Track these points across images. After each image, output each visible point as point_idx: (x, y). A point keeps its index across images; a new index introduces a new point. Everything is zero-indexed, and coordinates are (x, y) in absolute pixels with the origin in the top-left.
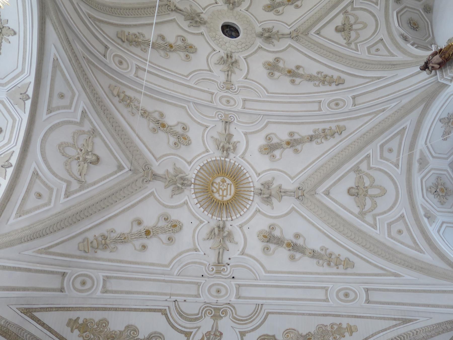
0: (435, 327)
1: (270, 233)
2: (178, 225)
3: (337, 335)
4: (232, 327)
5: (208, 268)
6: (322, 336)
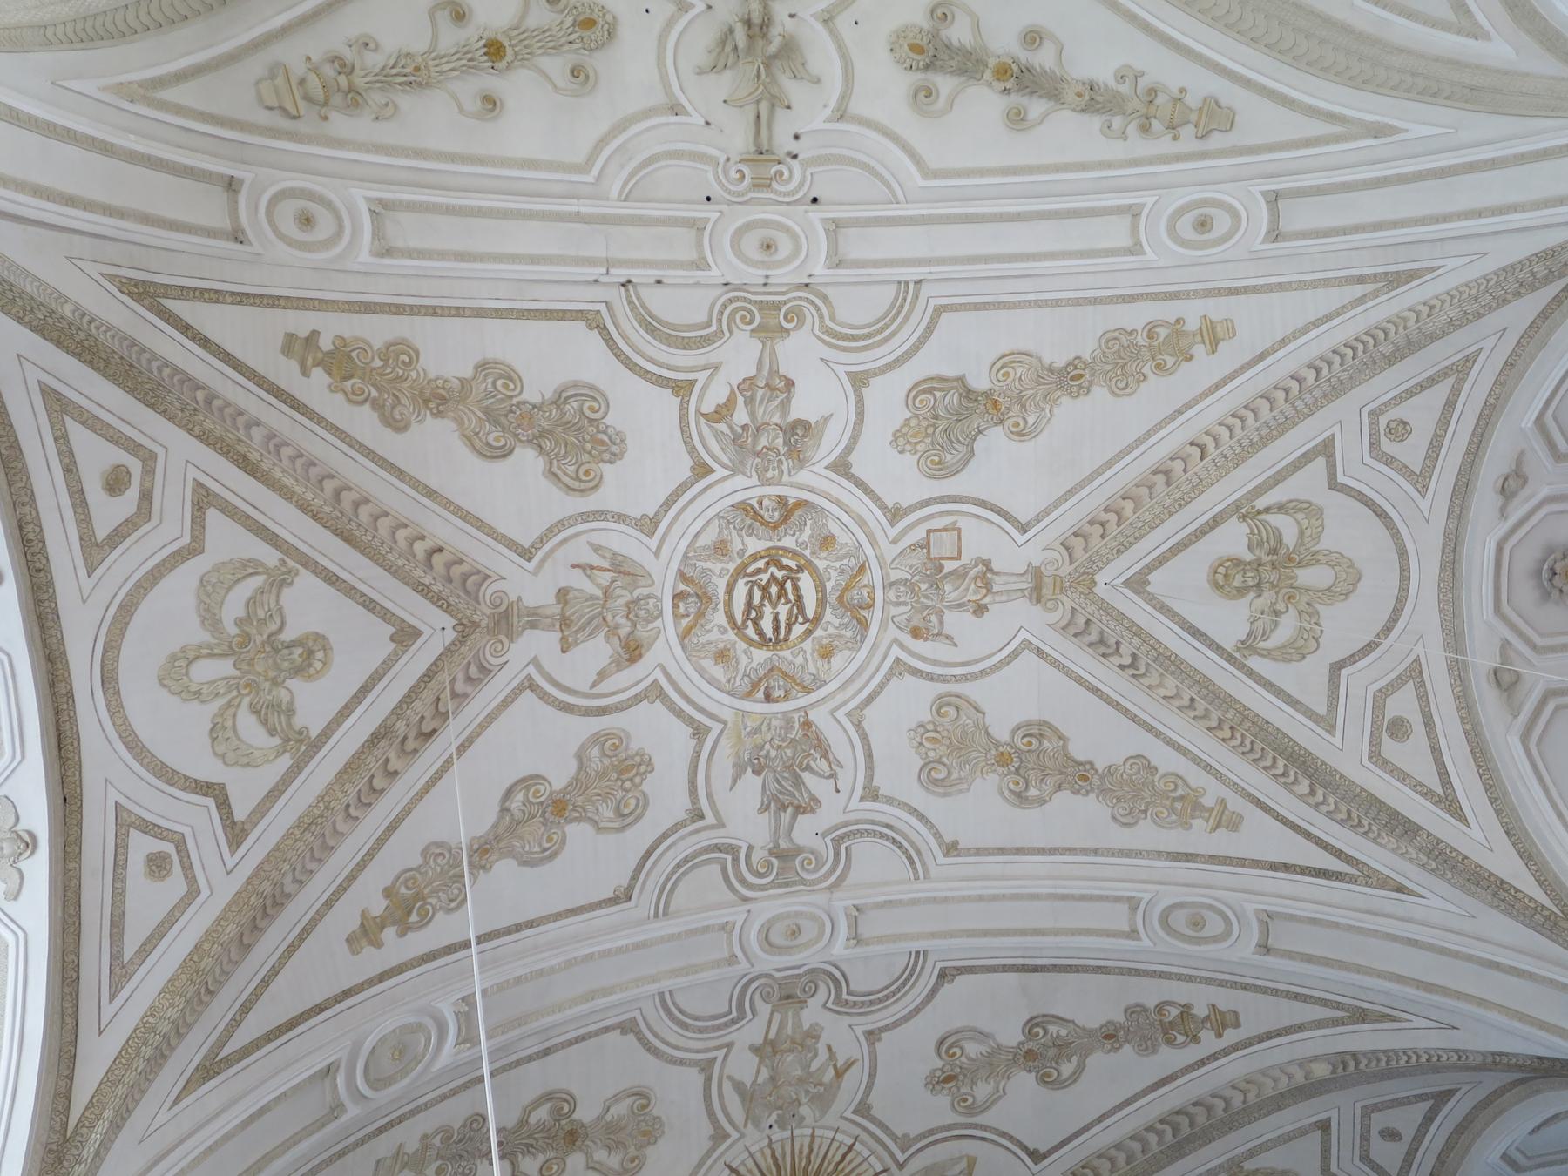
0: (1495, 278)
1: (935, 35)
2: (601, 21)
3: (1167, 358)
4: (822, 359)
5: (725, 172)
6: (1118, 363)
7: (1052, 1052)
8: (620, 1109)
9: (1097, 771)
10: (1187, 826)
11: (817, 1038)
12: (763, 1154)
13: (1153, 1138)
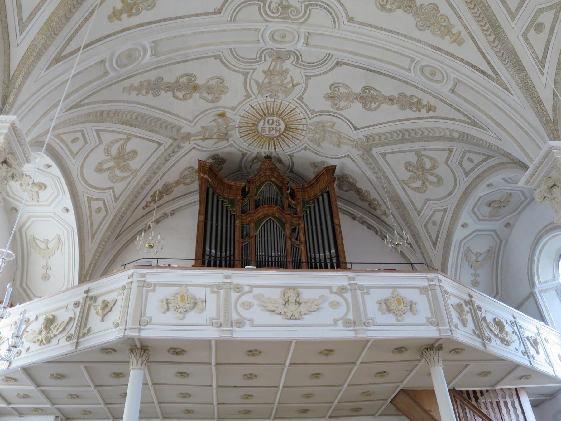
7: (370, 99)
8: (213, 82)
9: (416, 5)
10: (443, 38)
11: (288, 73)
12: (263, 105)
13: (395, 135)
